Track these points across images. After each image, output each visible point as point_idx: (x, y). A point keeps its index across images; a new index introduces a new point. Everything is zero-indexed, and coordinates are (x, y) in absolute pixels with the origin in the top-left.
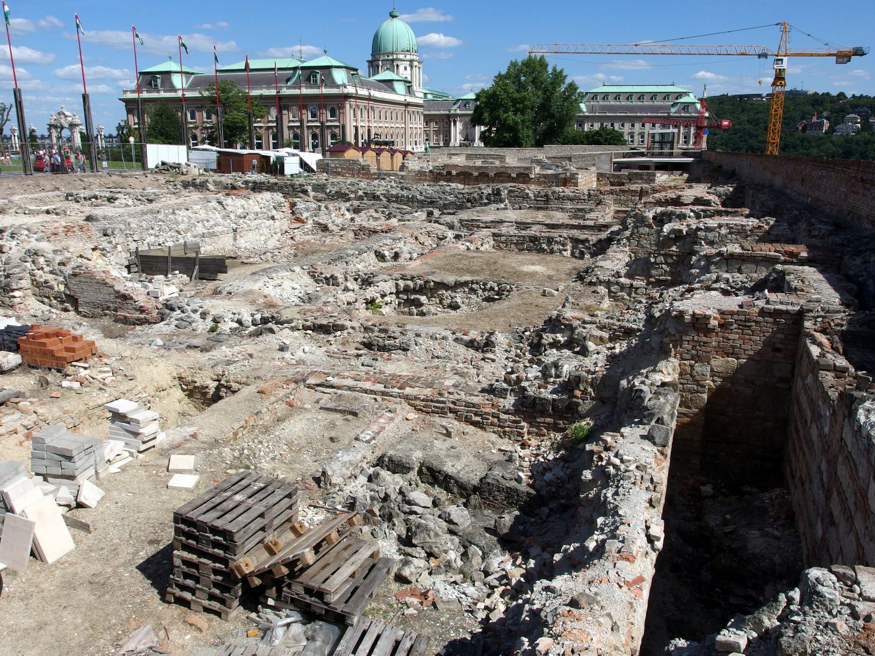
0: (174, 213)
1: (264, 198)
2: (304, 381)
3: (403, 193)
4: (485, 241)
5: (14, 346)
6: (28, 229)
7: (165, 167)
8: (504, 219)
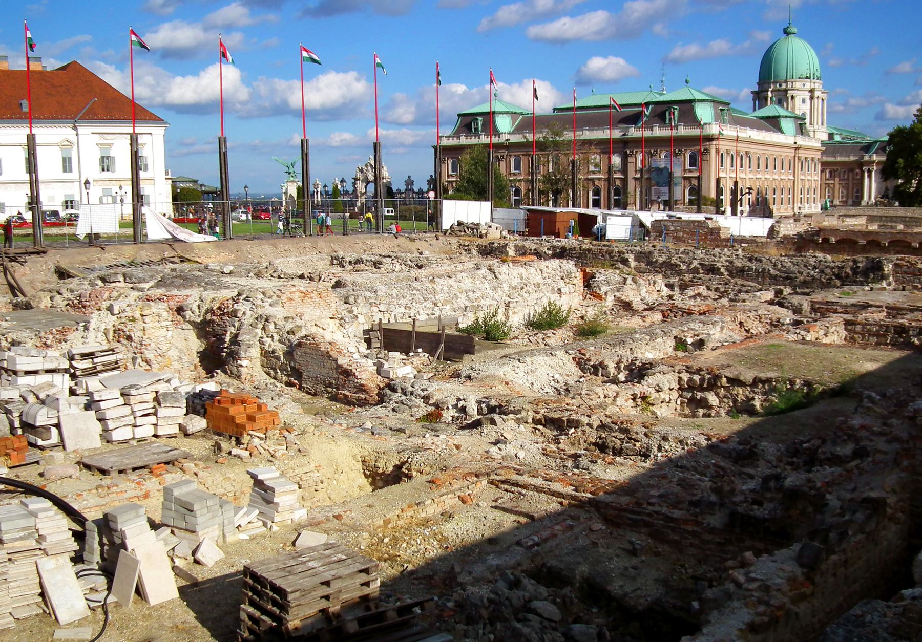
0: (433, 281)
1: (550, 265)
2: (488, 475)
3: (751, 265)
4: (832, 330)
5: (202, 411)
6: (263, 293)
7: (461, 228)
8: (871, 303)
